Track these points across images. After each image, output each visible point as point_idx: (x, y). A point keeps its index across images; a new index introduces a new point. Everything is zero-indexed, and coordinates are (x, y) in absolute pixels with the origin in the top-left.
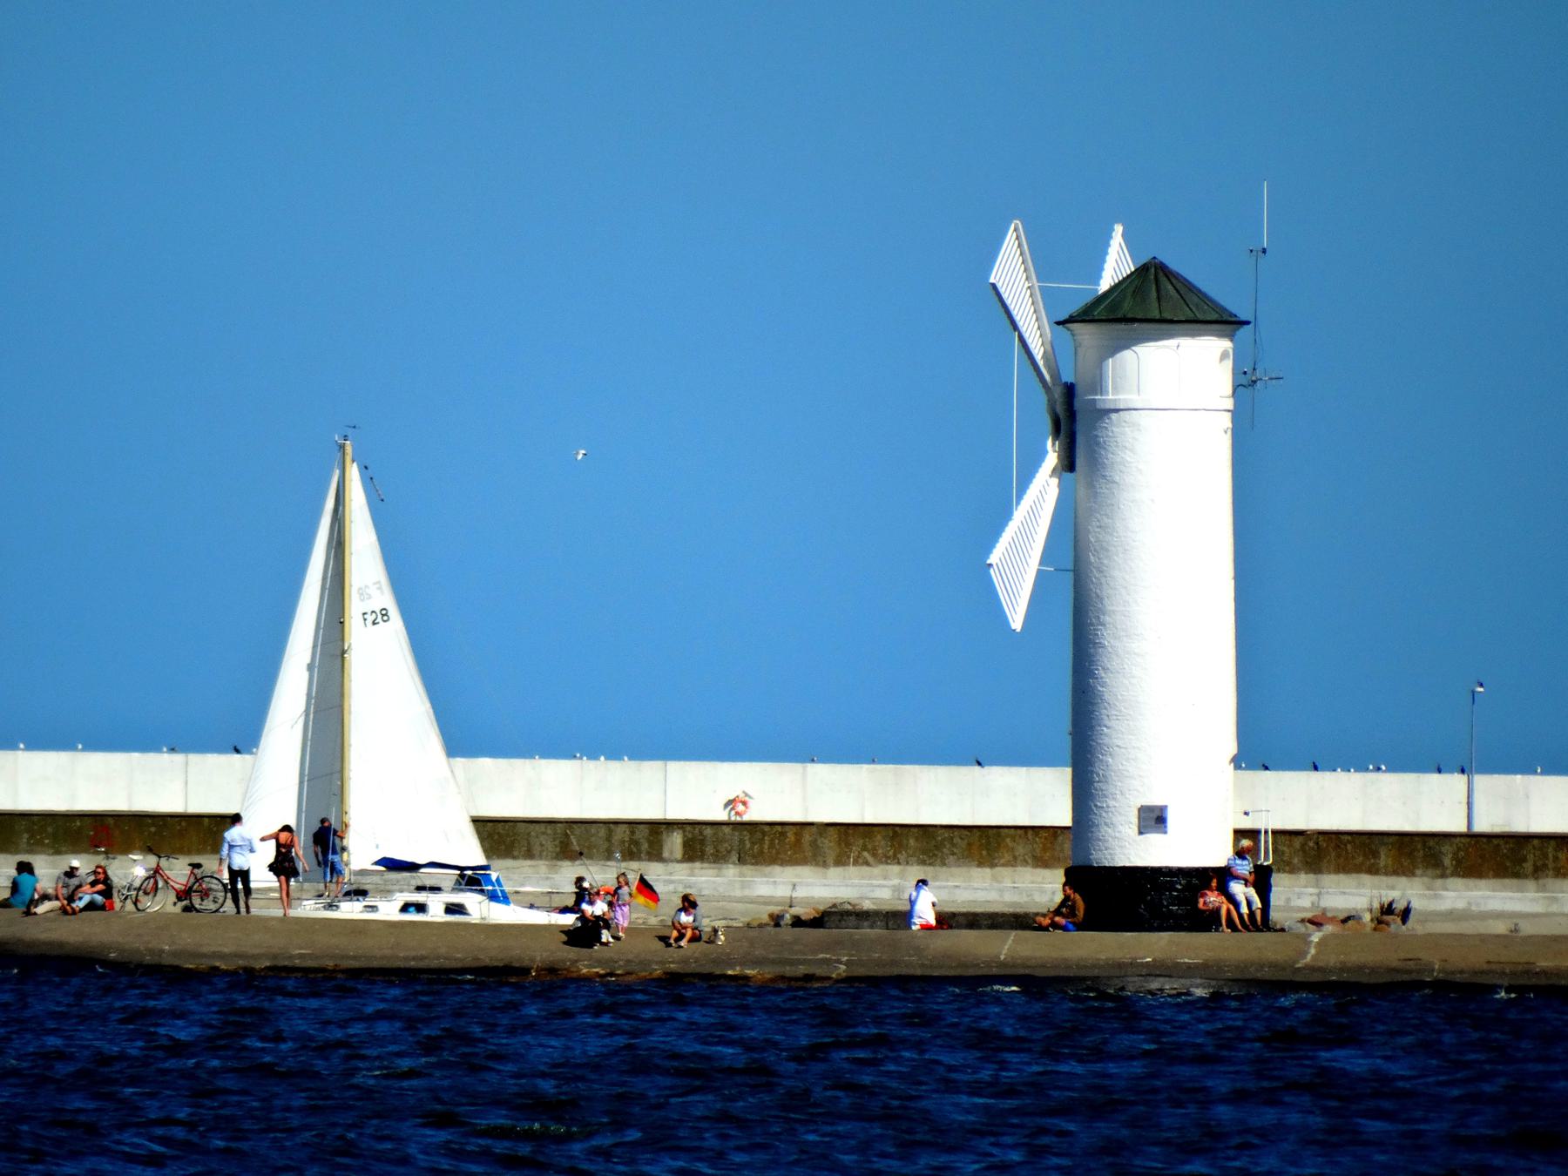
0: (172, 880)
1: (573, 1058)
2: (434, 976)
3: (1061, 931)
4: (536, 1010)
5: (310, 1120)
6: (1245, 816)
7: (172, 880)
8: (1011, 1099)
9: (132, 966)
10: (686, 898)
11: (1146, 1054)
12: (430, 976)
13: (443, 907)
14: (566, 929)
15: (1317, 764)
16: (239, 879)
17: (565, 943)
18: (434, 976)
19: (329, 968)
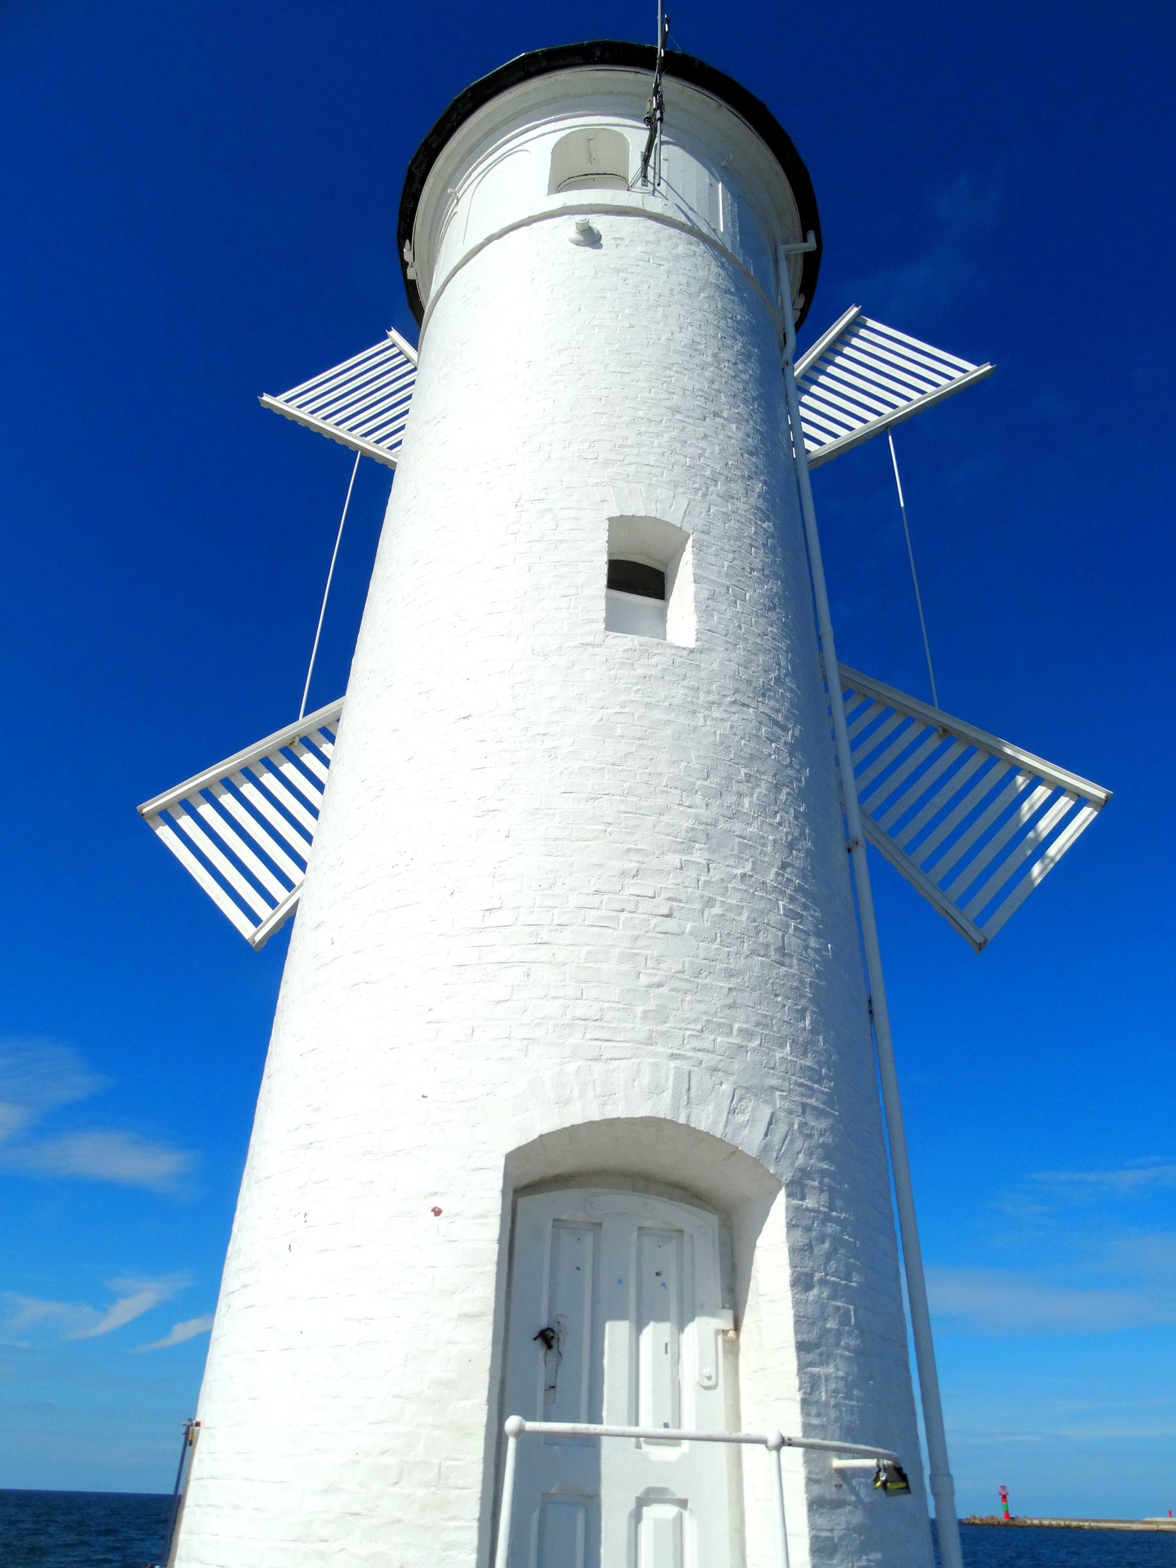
0: (640, 128)
1: (729, 282)
2: (752, 273)
3: (311, 429)
4: (725, 1091)
5: (110, 1556)
6: (658, 1277)
7: (640, 128)
8: (629, 148)
9: (861, 1346)
10: (433, 1210)
11: (713, 581)
12: (852, 1313)
13: (666, 1422)
14: (634, 1329)
15: (425, 1098)
16: (987, 367)
17: (578, 243)
18: (752, 273)
19: (1086, 1527)
